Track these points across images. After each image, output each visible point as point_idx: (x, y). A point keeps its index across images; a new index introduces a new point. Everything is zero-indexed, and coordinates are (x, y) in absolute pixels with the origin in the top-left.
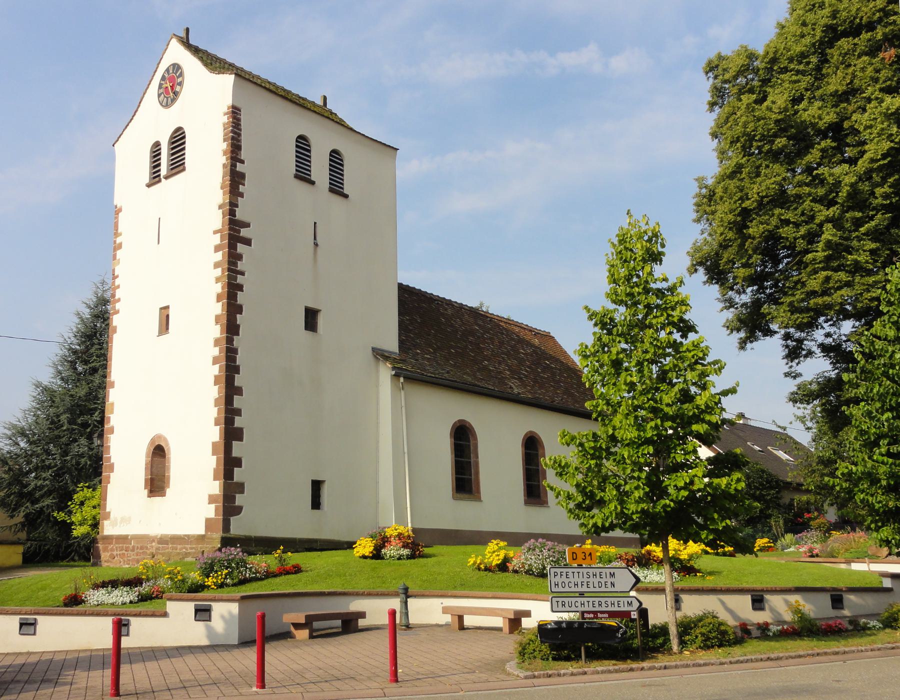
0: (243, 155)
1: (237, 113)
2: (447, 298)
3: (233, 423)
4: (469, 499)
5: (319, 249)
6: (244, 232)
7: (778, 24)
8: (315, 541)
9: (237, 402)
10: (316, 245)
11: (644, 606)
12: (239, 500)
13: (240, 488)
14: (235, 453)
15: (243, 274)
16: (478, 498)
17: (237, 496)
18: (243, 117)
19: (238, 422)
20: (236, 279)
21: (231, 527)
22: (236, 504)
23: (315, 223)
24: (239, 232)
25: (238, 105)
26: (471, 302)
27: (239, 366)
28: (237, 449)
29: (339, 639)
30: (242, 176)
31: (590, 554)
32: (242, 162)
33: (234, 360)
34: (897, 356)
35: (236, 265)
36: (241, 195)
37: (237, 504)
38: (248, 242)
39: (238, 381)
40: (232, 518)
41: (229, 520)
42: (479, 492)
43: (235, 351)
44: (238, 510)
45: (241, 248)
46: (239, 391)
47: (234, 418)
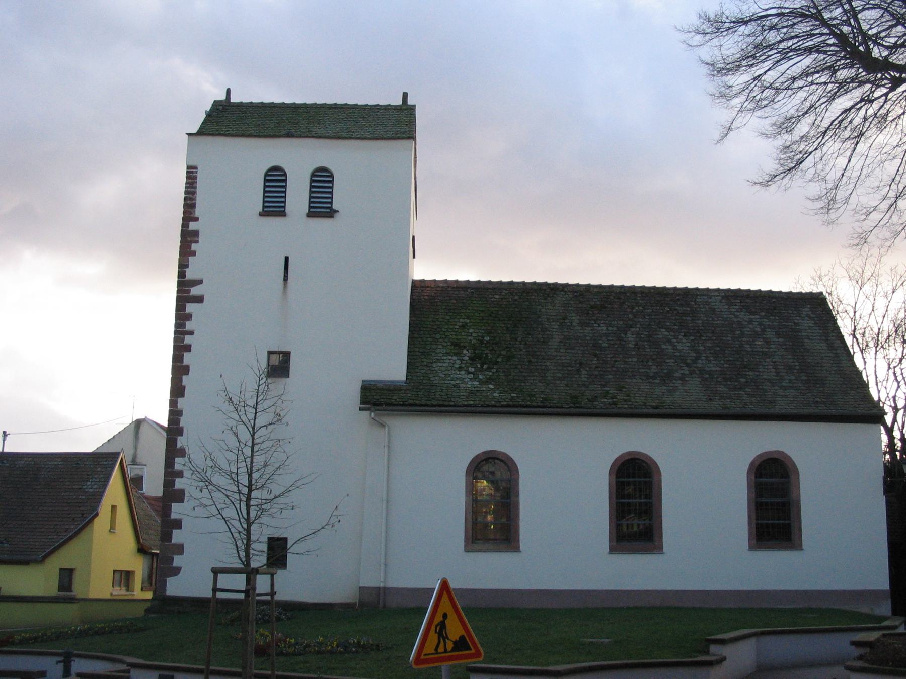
0: (198, 212)
1: (192, 172)
3: (170, 539)
4: (507, 551)
6: (195, 291)
7: (700, 16)
9: (187, 358)
11: (410, 102)
14: (179, 406)
15: (191, 333)
17: (187, 323)
18: (200, 176)
25: (192, 164)
27: (182, 428)
30: (196, 233)
32: (197, 219)
33: (178, 421)
34: (901, 270)
35: (184, 326)
36: (194, 254)
37: (181, 425)
38: (199, 299)
43: (180, 413)
45: (190, 308)
46: (182, 453)
47: (185, 323)
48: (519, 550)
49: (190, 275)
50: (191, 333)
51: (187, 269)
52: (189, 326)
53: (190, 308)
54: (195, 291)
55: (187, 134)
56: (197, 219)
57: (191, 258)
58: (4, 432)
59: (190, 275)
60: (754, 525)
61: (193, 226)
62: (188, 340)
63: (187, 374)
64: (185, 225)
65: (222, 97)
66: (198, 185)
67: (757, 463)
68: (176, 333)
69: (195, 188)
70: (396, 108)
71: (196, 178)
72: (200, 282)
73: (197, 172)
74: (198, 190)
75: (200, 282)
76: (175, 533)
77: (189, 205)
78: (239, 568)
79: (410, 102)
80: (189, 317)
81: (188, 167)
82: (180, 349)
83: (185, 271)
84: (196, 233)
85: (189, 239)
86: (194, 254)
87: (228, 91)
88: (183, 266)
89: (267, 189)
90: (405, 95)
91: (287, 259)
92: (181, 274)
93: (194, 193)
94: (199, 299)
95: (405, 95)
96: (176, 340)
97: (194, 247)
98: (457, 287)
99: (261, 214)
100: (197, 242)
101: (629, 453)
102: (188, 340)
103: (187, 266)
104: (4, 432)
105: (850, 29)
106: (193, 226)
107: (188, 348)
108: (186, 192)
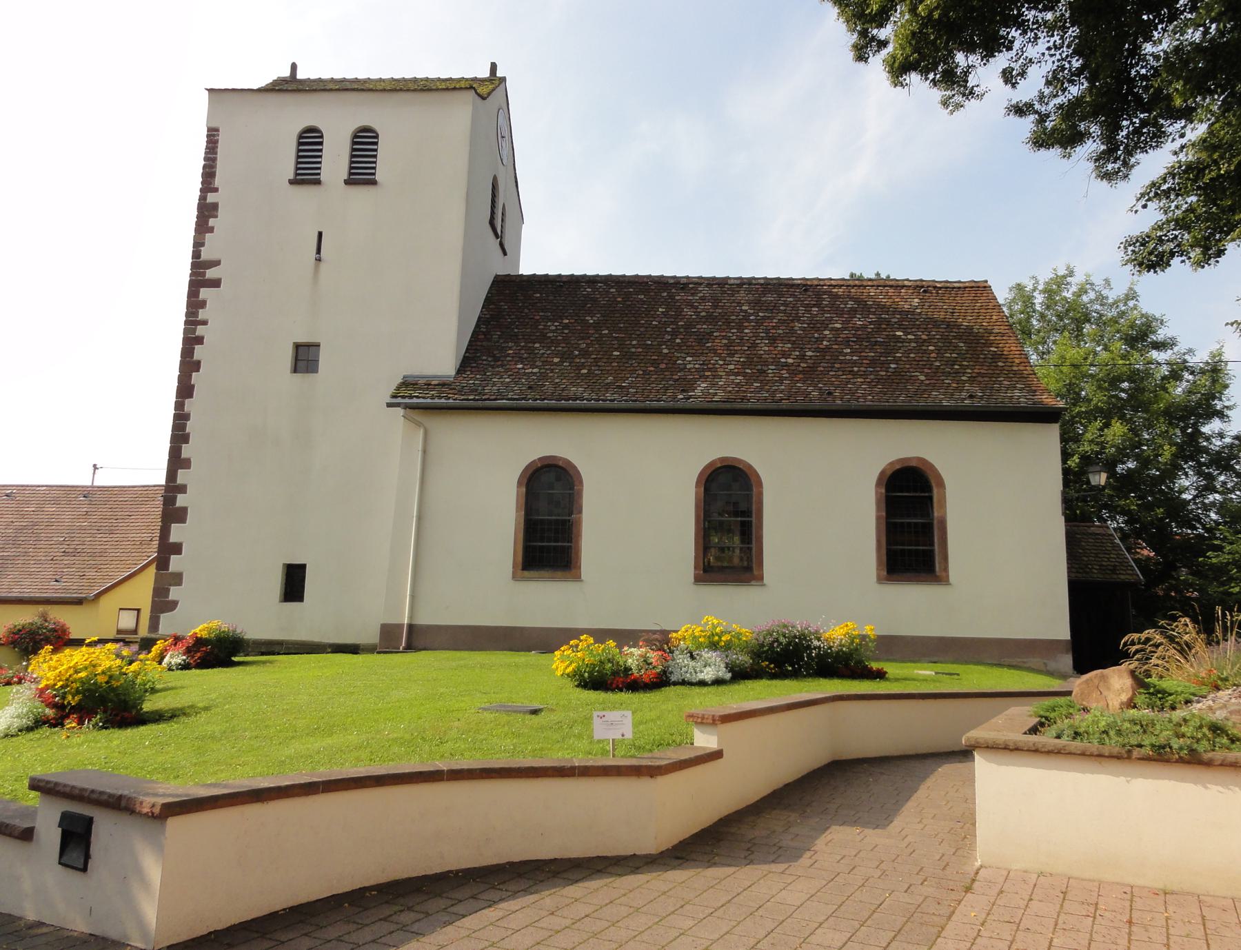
0: (217, 182)
1: (214, 135)
2: (539, 273)
4: (565, 579)
5: (323, 265)
6: (211, 274)
8: (280, 643)
10: (319, 260)
12: (174, 593)
13: (178, 579)
15: (205, 323)
16: (578, 578)
18: (222, 139)
19: (181, 500)
20: (195, 330)
21: (160, 626)
22: (170, 598)
23: (320, 234)
24: (204, 274)
25: (214, 125)
26: (595, 273)
27: (188, 435)
28: (177, 533)
29: (78, 873)
30: (215, 206)
31: (780, 848)
32: (216, 190)
33: (183, 427)
35: (195, 314)
36: (211, 230)
38: (216, 283)
39: (186, 451)
40: (162, 615)
41: (159, 617)
42: (524, 579)
44: (173, 605)
46: (186, 464)
47: (176, 497)
48: (580, 577)
49: (206, 255)
50: (205, 323)
51: (202, 248)
52: (202, 314)
53: (204, 293)
54: (211, 274)
55: (206, 89)
56: (216, 190)
57: (208, 235)
58: (95, 466)
59: (206, 255)
60: (884, 551)
61: (211, 198)
62: (200, 330)
63: (198, 370)
64: (203, 198)
65: (286, 73)
66: (219, 150)
67: (889, 473)
68: (186, 323)
69: (216, 153)
70: (483, 80)
71: (217, 142)
72: (216, 263)
73: (218, 135)
74: (219, 156)
75: (216, 263)
76: (174, 559)
77: (209, 174)
78: (894, 664)
79: (499, 74)
80: (203, 304)
81: (209, 130)
82: (191, 342)
83: (201, 251)
84: (215, 206)
85: (206, 213)
86: (211, 230)
87: (294, 67)
88: (198, 245)
89: (301, 154)
90: (494, 67)
91: (320, 234)
92: (196, 254)
93: (214, 160)
94: (216, 283)
95: (494, 67)
96: (186, 331)
97: (212, 222)
98: (545, 281)
99: (292, 182)
100: (216, 217)
101: (722, 459)
102: (200, 330)
103: (203, 245)
104: (95, 466)
105: (1037, 116)
106: (211, 198)
107: (200, 340)
108: (205, 159)
